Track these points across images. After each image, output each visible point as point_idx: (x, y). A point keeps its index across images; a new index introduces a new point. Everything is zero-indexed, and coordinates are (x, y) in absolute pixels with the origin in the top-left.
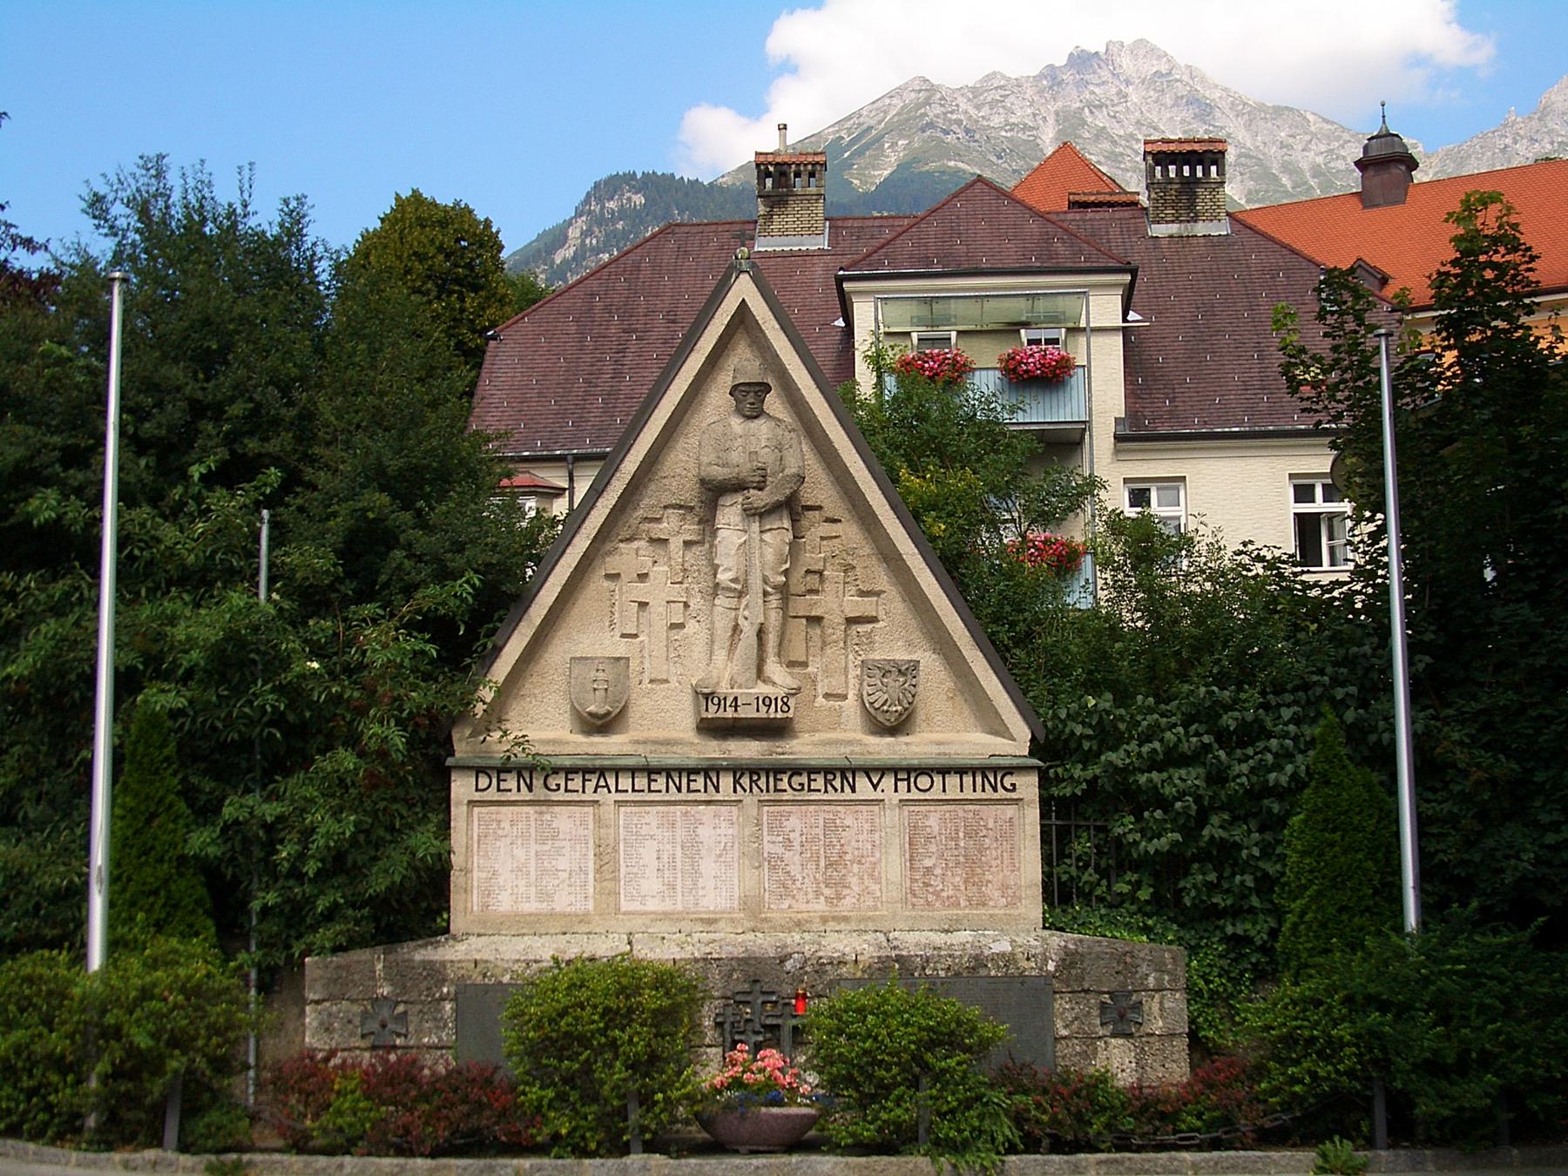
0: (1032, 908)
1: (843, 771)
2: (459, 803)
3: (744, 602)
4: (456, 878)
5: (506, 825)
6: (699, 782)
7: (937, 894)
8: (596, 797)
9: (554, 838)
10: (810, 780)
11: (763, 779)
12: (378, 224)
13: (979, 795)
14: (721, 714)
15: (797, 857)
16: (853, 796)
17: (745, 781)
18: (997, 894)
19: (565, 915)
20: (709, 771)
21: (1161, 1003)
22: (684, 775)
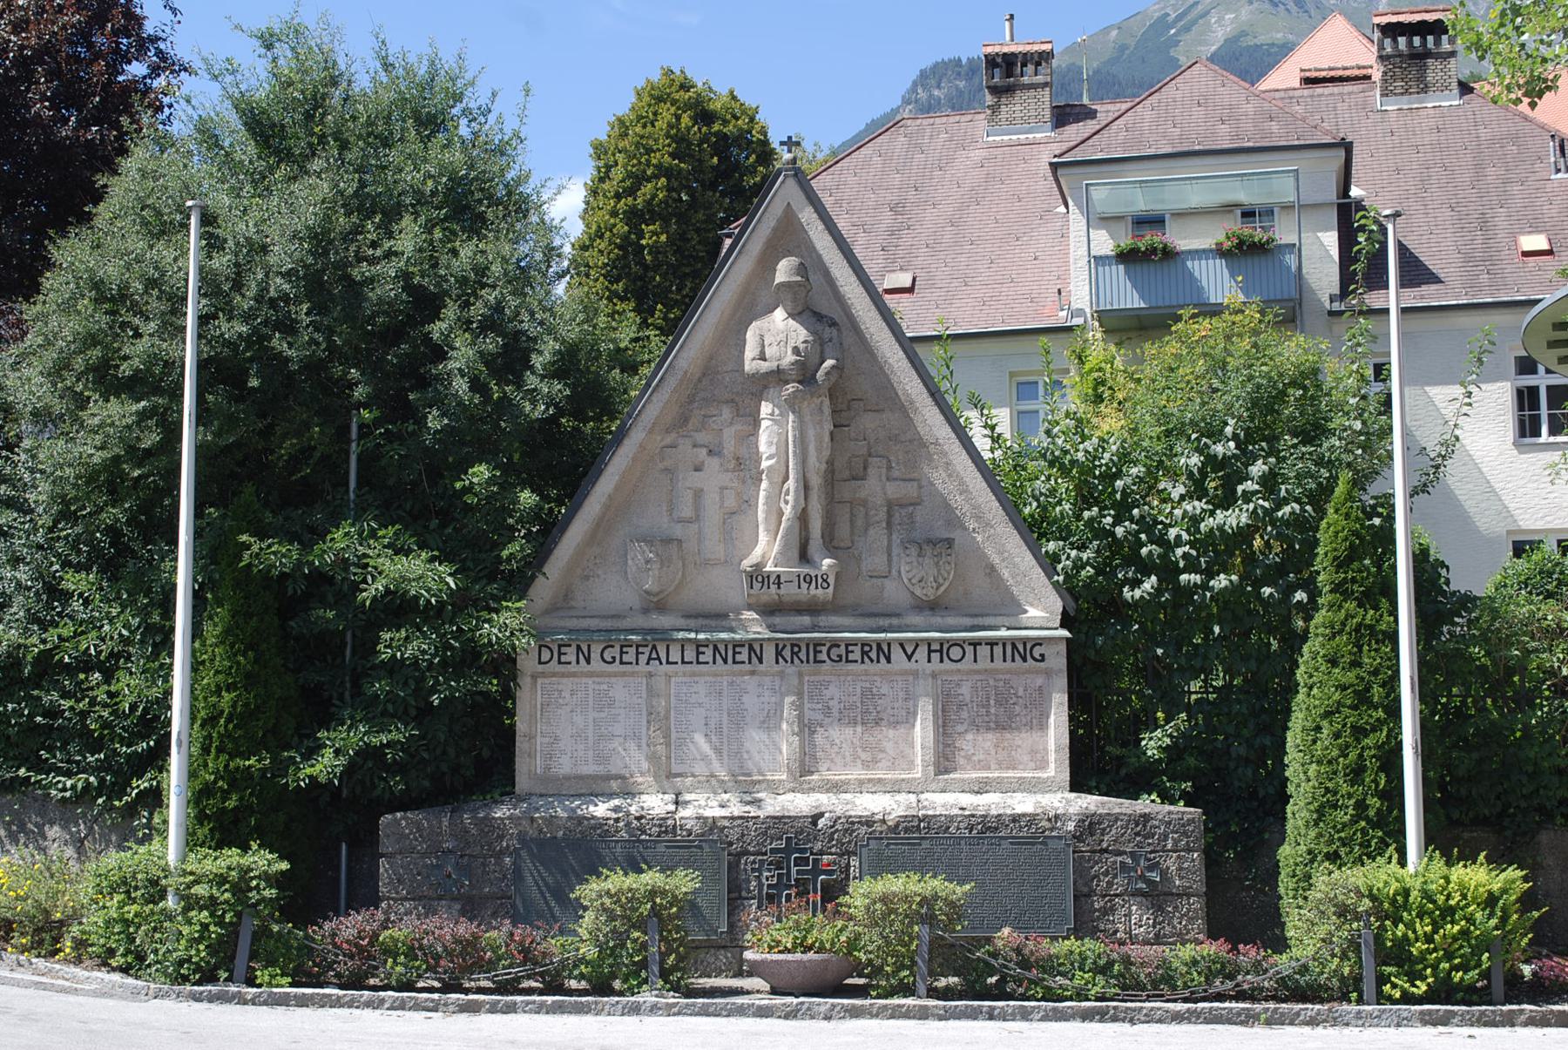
4: (521, 744)
5: (566, 694)
10: (622, 652)
12: (55, 255)
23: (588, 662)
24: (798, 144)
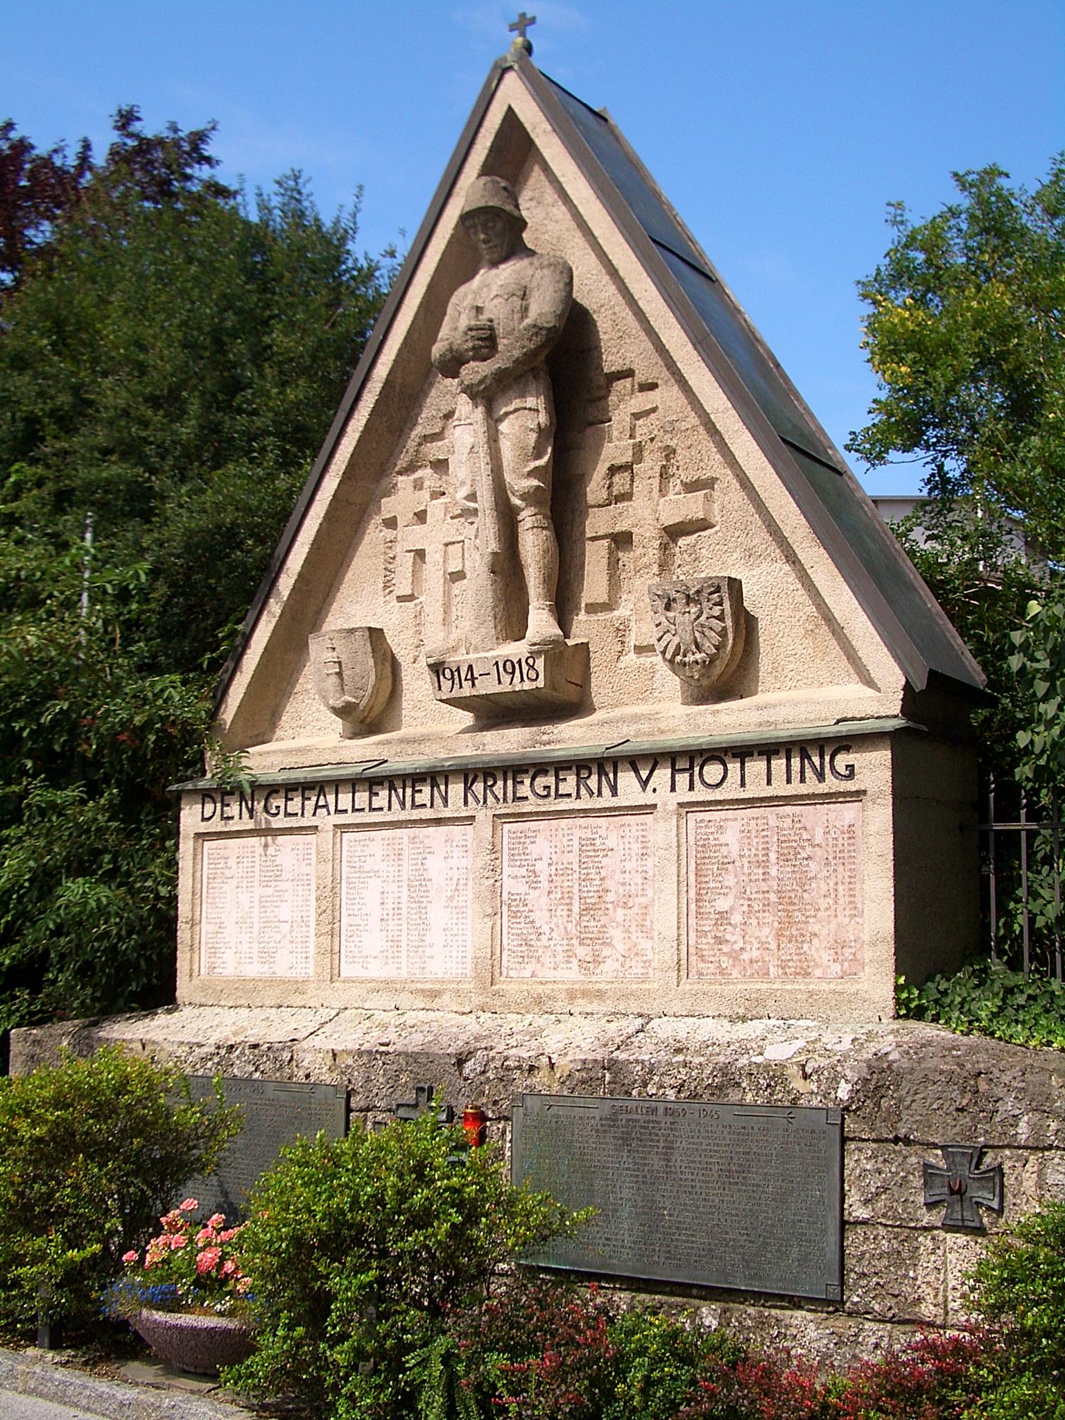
0: (878, 981)
2: (186, 837)
10: (558, 780)
11: (500, 783)
12: (104, 141)
13: (796, 788)
15: (544, 900)
16: (614, 802)
18: (826, 956)
21: (1040, 1174)
22: (409, 783)
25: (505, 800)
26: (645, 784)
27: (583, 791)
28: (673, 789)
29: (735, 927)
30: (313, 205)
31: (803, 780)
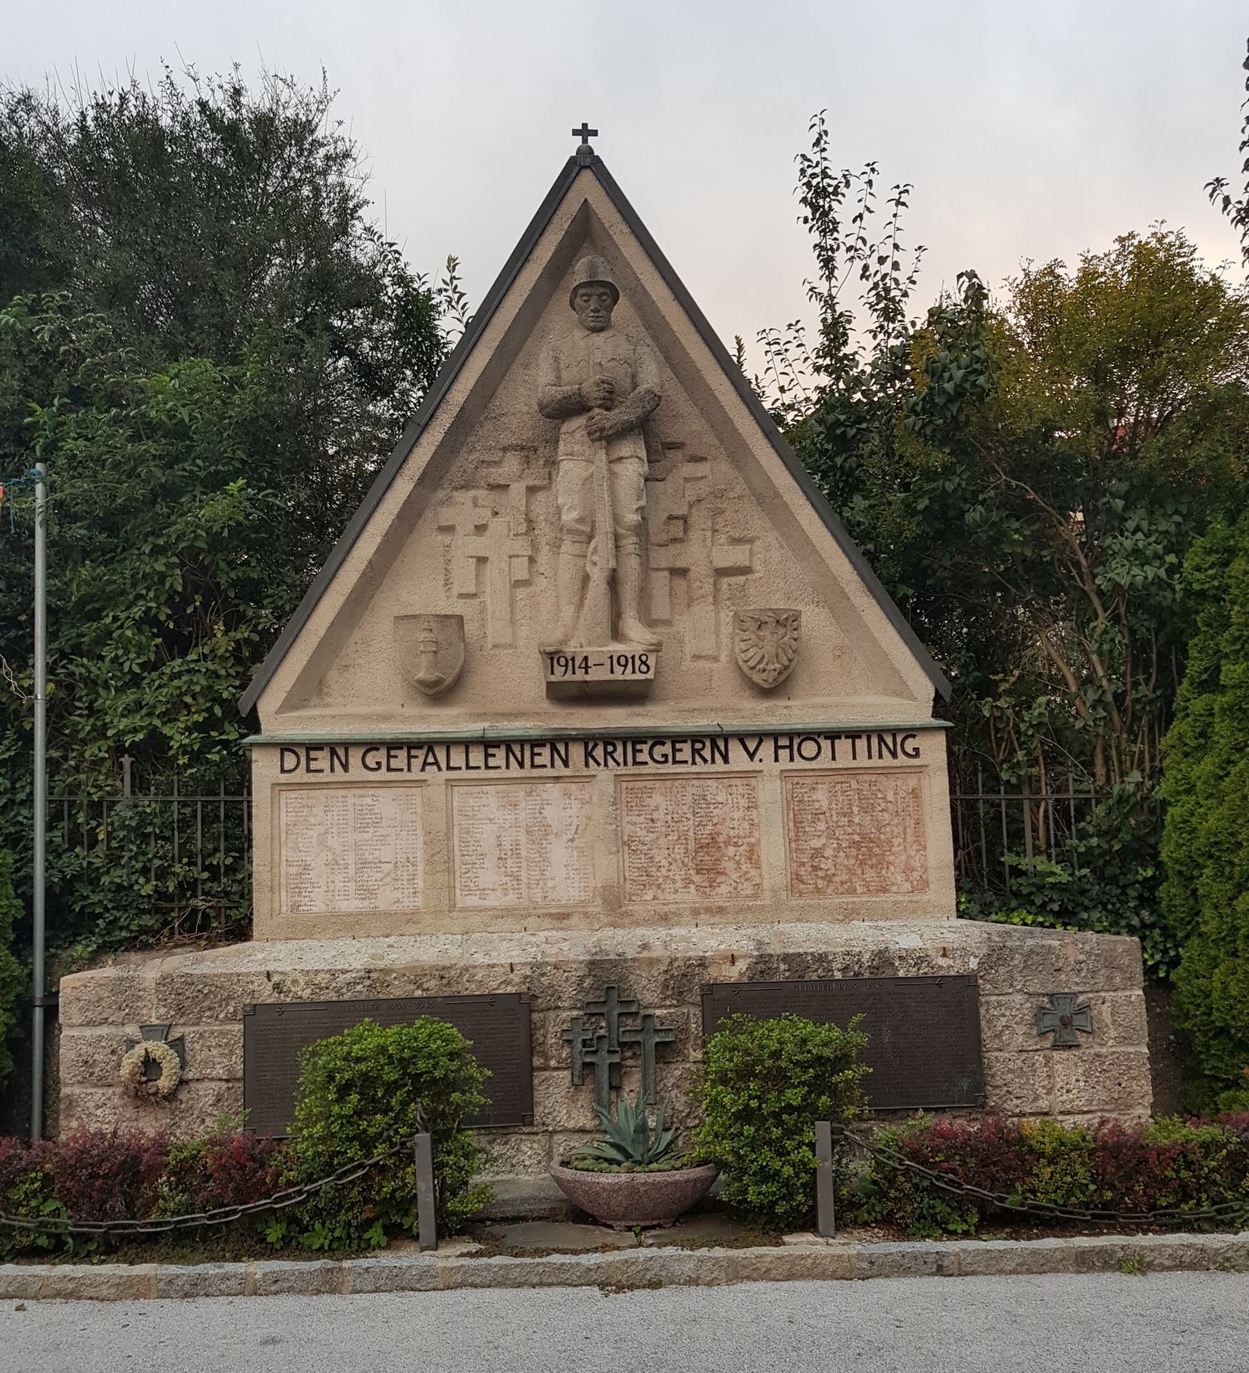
0: (943, 889)
1: (713, 738)
3: (593, 544)
6: (545, 755)
7: (828, 879)
8: (423, 776)
9: (376, 824)
10: (389, 757)
14: (569, 677)
16: (726, 768)
17: (599, 753)
18: (899, 878)
19: (389, 914)
20: (555, 742)
23: (345, 767)
24: (595, 133)
25: (625, 764)
26: (752, 756)
27: (698, 759)
28: (776, 760)
29: (827, 858)
30: (390, 252)
31: (881, 756)
